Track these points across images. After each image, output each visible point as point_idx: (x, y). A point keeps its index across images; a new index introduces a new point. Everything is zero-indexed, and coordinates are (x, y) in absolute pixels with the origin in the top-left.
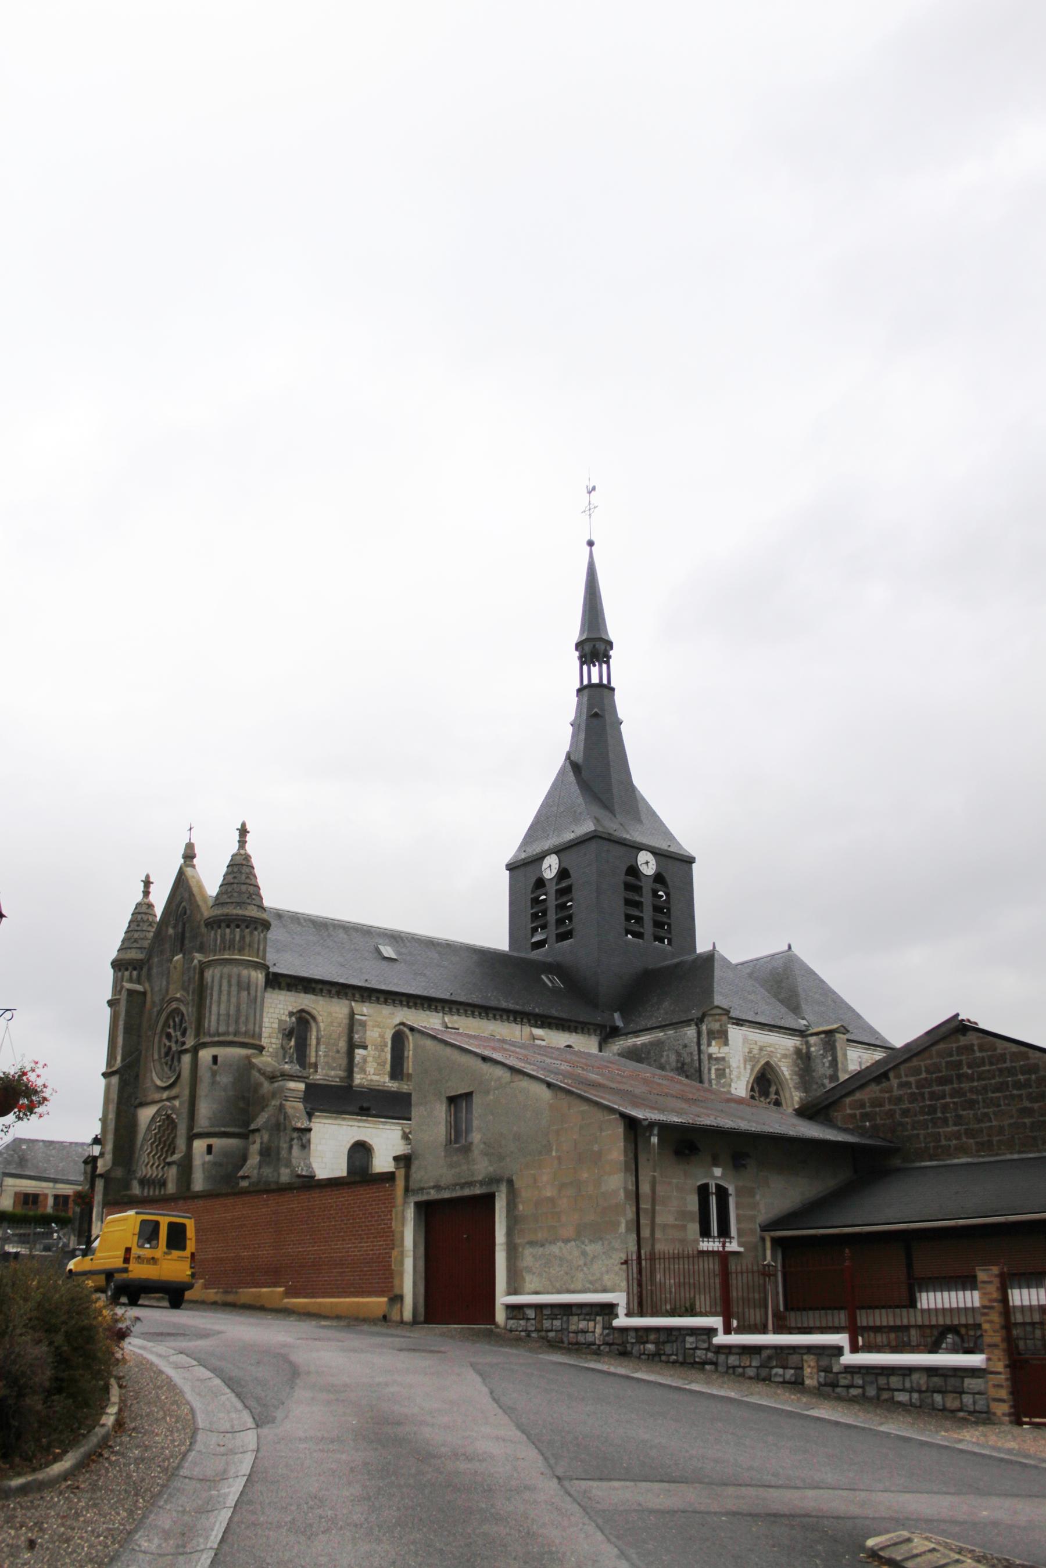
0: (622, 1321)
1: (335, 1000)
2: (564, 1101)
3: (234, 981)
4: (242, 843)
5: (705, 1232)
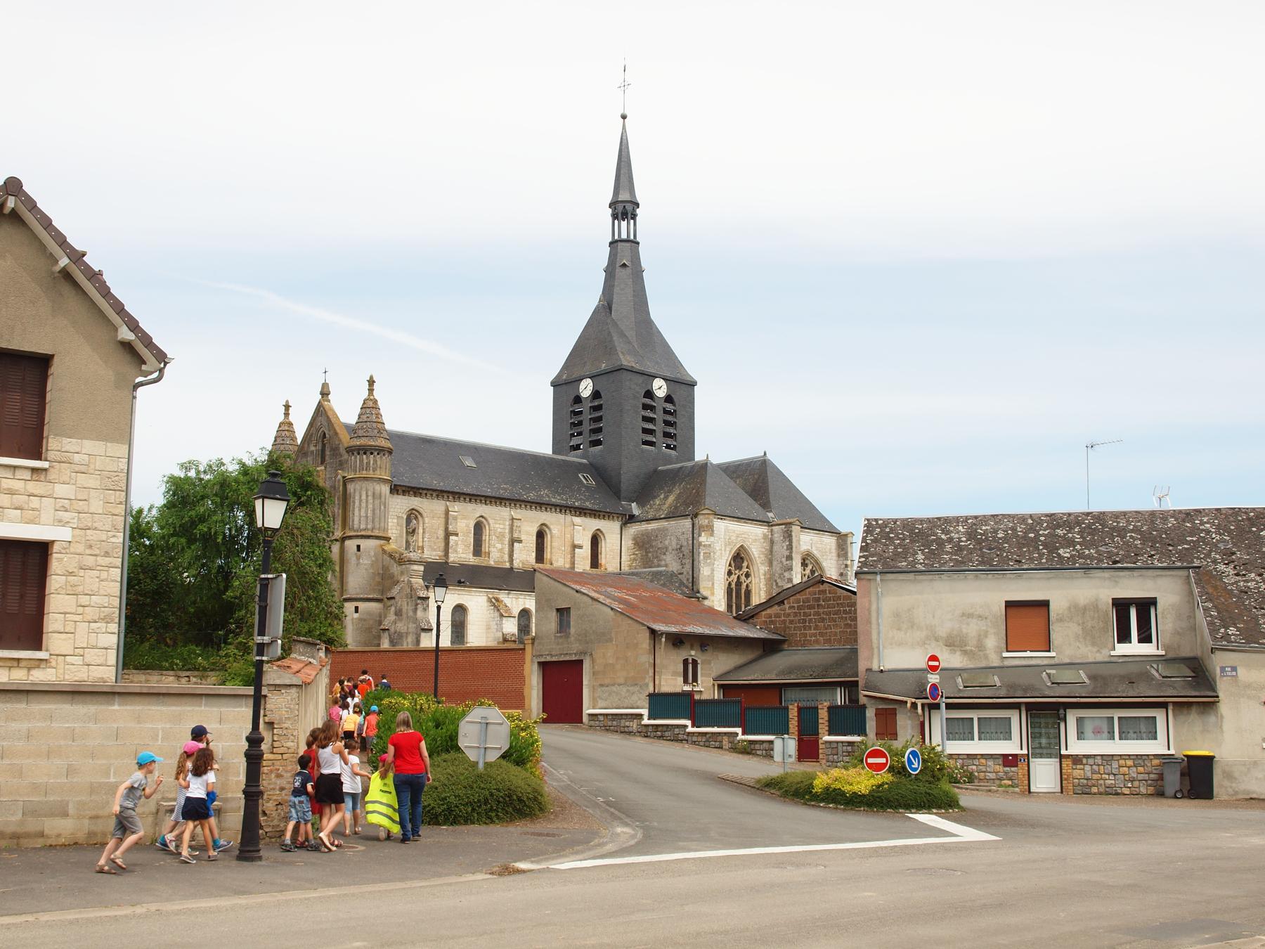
0: (646, 721)
1: (435, 501)
2: (620, 618)
3: (370, 493)
4: (371, 390)
5: (686, 681)
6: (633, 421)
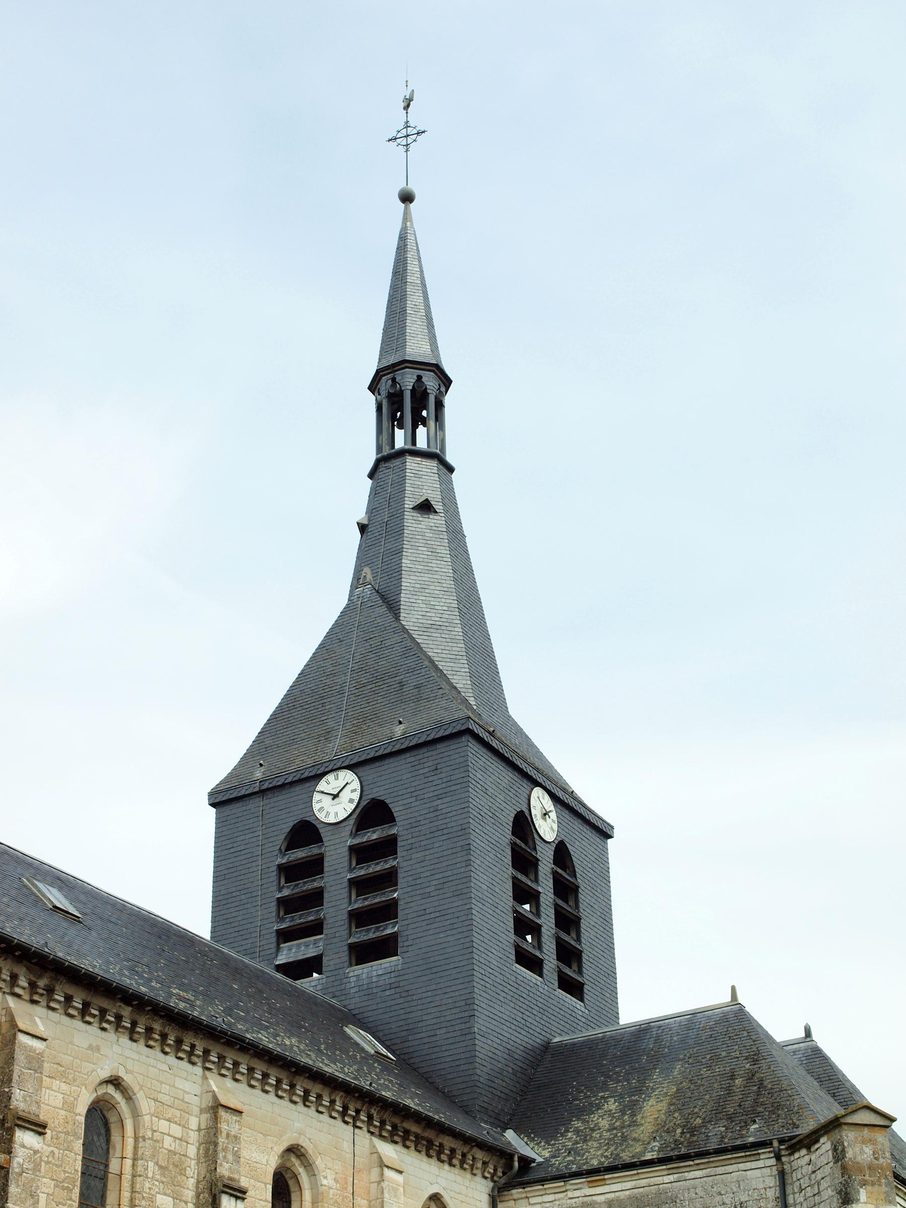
6: (493, 875)
